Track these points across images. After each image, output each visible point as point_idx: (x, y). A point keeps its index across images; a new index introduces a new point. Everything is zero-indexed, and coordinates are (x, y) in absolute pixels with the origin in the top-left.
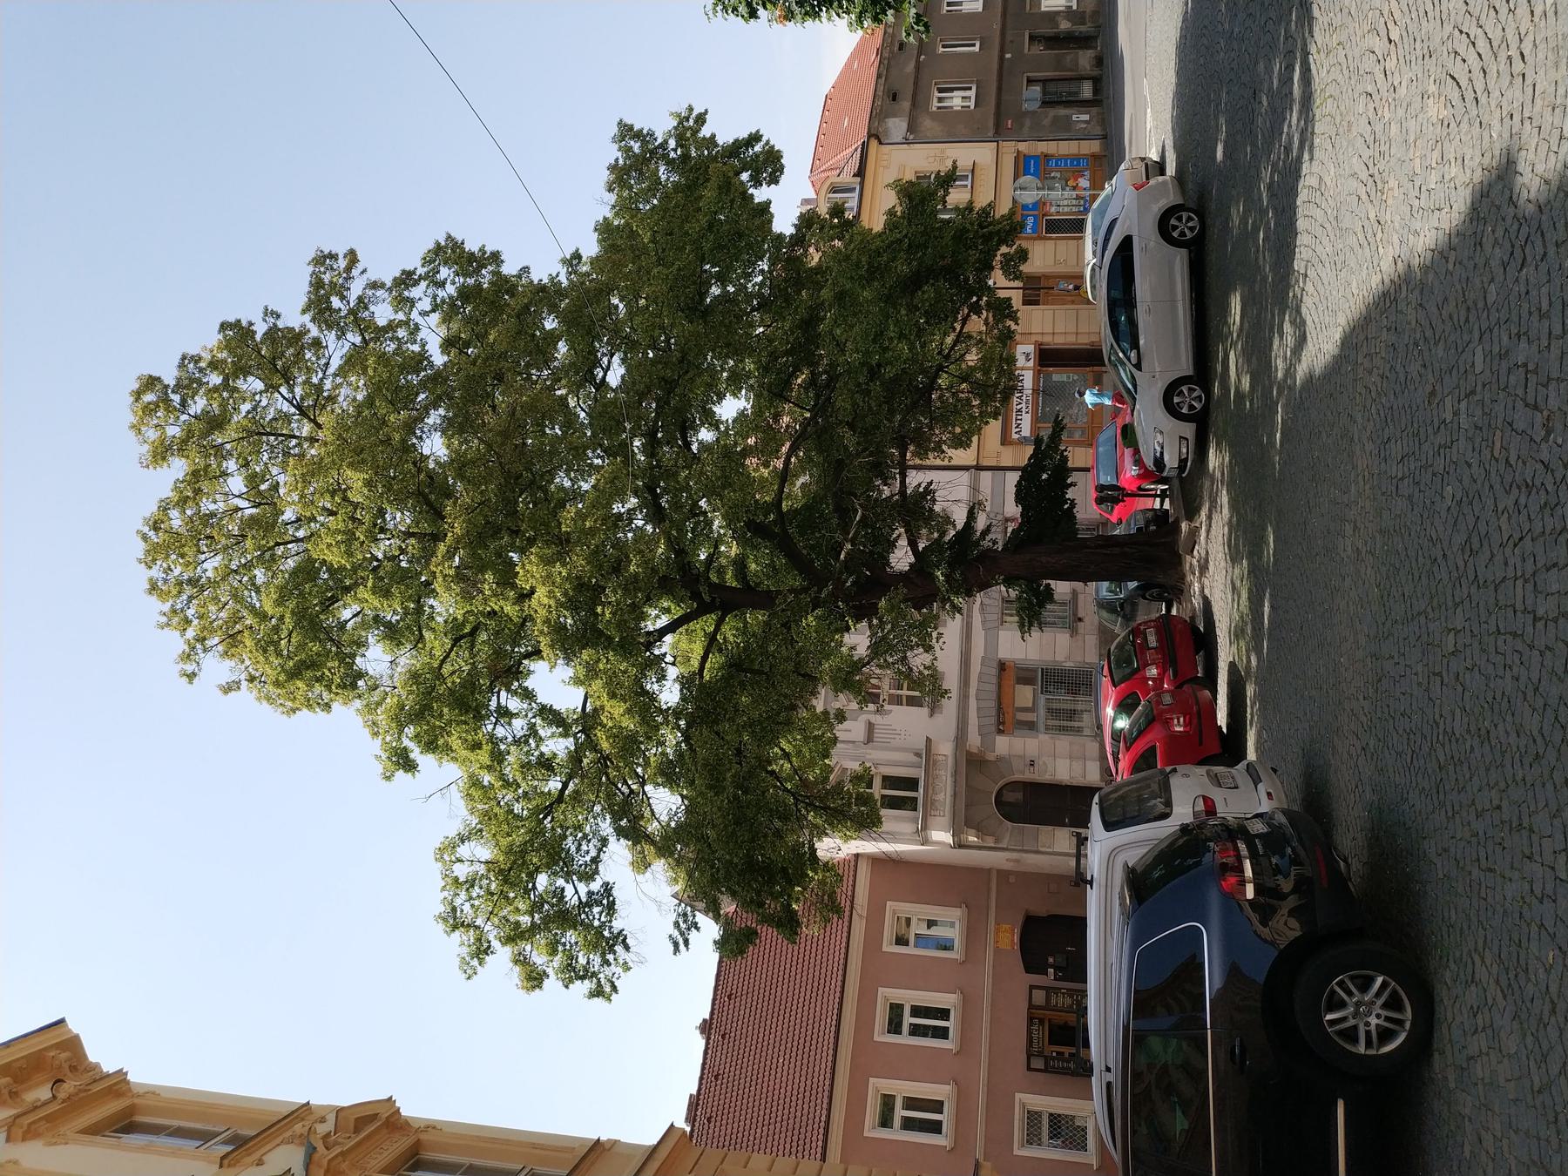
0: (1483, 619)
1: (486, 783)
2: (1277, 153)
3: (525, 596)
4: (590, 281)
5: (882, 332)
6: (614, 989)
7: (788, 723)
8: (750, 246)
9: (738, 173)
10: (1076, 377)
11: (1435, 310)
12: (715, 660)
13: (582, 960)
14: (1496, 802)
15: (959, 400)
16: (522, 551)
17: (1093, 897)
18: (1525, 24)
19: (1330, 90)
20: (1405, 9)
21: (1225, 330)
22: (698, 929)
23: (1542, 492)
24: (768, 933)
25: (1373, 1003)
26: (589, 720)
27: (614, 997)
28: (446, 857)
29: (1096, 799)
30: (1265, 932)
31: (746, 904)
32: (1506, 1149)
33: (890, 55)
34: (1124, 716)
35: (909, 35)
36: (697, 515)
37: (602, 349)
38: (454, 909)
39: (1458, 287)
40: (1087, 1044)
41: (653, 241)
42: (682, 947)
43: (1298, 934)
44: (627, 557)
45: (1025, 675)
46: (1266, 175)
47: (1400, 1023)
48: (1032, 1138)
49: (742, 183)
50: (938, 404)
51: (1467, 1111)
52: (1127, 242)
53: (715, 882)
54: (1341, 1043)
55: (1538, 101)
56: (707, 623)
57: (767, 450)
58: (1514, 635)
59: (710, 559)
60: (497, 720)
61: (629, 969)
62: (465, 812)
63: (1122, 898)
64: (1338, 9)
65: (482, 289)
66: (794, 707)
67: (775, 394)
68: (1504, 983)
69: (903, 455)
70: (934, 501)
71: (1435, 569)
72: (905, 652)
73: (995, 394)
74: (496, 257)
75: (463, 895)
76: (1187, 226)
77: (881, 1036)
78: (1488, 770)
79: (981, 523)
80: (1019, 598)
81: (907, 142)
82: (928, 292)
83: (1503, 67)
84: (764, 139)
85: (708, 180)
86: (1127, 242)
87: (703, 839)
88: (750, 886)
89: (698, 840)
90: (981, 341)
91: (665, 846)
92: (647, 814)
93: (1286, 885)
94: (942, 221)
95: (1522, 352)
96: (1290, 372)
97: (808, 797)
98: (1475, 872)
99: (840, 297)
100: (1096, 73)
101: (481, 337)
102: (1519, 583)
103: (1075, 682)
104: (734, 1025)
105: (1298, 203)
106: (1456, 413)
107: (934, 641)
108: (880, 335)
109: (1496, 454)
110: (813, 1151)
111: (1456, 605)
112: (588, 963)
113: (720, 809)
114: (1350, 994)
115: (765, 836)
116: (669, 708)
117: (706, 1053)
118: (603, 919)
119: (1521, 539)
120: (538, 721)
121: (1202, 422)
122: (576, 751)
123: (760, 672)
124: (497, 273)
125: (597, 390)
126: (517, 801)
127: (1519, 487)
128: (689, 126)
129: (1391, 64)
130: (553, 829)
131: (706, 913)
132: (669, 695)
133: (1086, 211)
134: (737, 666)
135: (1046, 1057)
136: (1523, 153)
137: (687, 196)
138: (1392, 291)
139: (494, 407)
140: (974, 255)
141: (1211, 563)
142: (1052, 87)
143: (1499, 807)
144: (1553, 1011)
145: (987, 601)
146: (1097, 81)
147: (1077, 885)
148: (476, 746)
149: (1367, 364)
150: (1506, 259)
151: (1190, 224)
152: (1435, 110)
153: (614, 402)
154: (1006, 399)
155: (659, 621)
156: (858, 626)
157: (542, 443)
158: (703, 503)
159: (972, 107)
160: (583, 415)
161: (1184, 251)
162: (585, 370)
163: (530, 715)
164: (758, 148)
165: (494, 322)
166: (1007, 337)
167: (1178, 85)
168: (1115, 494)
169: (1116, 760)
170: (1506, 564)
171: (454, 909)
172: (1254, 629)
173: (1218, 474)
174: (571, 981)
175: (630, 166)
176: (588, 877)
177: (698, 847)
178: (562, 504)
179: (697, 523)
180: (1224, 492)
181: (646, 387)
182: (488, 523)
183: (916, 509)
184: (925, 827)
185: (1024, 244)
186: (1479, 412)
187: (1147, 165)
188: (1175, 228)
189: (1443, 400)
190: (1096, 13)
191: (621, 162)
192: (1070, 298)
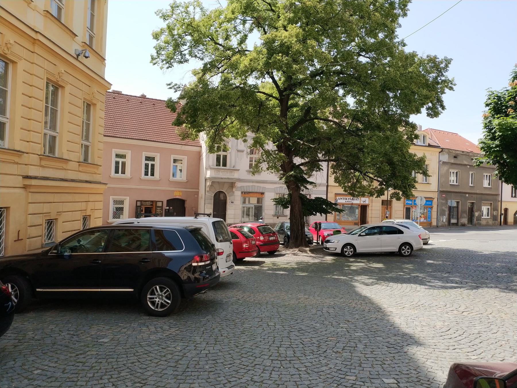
0: (278, 333)
1: (221, 17)
2: (429, 278)
3: (285, 28)
4: (396, 50)
5: (374, 152)
6: (155, 64)
7: (243, 123)
8: (406, 106)
9: (431, 102)
10: (357, 217)
11: (375, 322)
12: (263, 97)
13: (163, 53)
14: (223, 335)
15: (350, 179)
16: (301, 27)
17: (191, 219)
18: (465, 350)
19: (448, 295)
20: (473, 317)
21: (371, 262)
22: (175, 92)
23: (317, 350)
24: (175, 116)
25: (162, 300)
26: (242, 52)
27: (152, 64)
28: (195, 3)
29: (222, 220)
30: (183, 268)
31: (184, 108)
32: (123, 335)
33: (469, 155)
34: (248, 230)
35: (476, 159)
36: (313, 89)
37: (372, 54)
38: (178, 7)
39: (382, 329)
40: (145, 217)
41: (409, 72)
42: (169, 86)
43: (182, 278)
44: (299, 64)
45: (259, 201)
46: (421, 275)
47: (157, 307)
48: (116, 202)
49: (428, 103)
50: (349, 172)
51: (132, 325)
52: (401, 232)
53: (190, 97)
54: (150, 291)
55: (440, 353)
56: (276, 94)
57: (335, 114)
58: (274, 341)
59: (298, 94)
60: (242, 20)
61: (161, 69)
62: (210, 9)
63: (192, 226)
64: (475, 297)
65: (394, 10)
66: (248, 124)
67: (355, 116)
68: (170, 336)
69: (332, 160)
70: (317, 171)
71: (294, 320)
72: (267, 161)
73: (352, 190)
74: (405, 15)
75: (183, 10)
76: (406, 251)
77: (145, 154)
78: (233, 333)
79: (309, 186)
80: (284, 198)
81: (439, 161)
82: (387, 168)
83: (451, 344)
84: (443, 111)
85: (429, 91)
86: (401, 232)
87: (204, 93)
88: (190, 110)
89: (204, 92)
90: (370, 186)
91: (201, 80)
92: (212, 74)
93: (197, 275)
94: (412, 172)
95: (361, 346)
96: (357, 281)
97: (219, 130)
98: (202, 329)
99: (387, 138)
100: (459, 224)
101: (376, 10)
102: (290, 343)
103: (258, 212)
104: (145, 106)
105: (412, 284)
106: (342, 327)
107: (270, 171)
108: (373, 151)
109: (329, 338)
110: (106, 132)
111: (283, 326)
112: (162, 55)
113: (214, 99)
114: (165, 293)
115: (206, 115)
116: (247, 80)
117: (135, 97)
118: (177, 59)
119: (303, 344)
120: (242, 34)
121: (342, 254)
122: (232, 48)
123: (259, 113)
124: (399, 15)
125: (358, 53)
126: (215, 28)
127: (319, 344)
128: (449, 84)
129: (455, 312)
130: (206, 41)
131: (181, 95)
132: (251, 81)
133: (413, 220)
134: (261, 104)
135: (141, 206)
136: (424, 348)
137: (424, 84)
138: (381, 311)
139: (351, 15)
140: (400, 183)
141: (296, 257)
142: (455, 209)
143: (222, 336)
144: (163, 348)
145: (283, 189)
146: (456, 224)
147: (195, 214)
148: (233, 13)
149: (358, 303)
150: (390, 343)
151: (406, 252)
152: (439, 324)
153: (353, 59)
154: (350, 194)
155: (276, 76)
156: (275, 147)
157: (339, 33)
158: (317, 91)
159: (450, 183)
160: (349, 48)
161: (397, 250)
162: (364, 49)
163: (244, 31)
164: (440, 109)
165: (382, 15)
166: (371, 194)
167: (453, 250)
168: (318, 228)
169: (234, 227)
170: (295, 340)
171: (178, 7)
172: (276, 269)
173: (324, 259)
174: (156, 49)
175: (436, 63)
176: (190, 54)
177: (202, 92)
178: (317, 40)
179: (310, 89)
180: (318, 261)
181: (358, 70)
182: (311, 14)
183: (314, 165)
184: (211, 169)
185: (402, 200)
186: (342, 334)
187: (427, 239)
188: (405, 247)
189: (346, 324)
190: (480, 224)
191: (437, 60)
192: (383, 215)
